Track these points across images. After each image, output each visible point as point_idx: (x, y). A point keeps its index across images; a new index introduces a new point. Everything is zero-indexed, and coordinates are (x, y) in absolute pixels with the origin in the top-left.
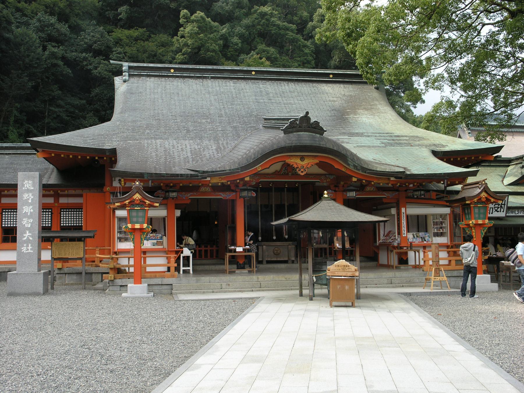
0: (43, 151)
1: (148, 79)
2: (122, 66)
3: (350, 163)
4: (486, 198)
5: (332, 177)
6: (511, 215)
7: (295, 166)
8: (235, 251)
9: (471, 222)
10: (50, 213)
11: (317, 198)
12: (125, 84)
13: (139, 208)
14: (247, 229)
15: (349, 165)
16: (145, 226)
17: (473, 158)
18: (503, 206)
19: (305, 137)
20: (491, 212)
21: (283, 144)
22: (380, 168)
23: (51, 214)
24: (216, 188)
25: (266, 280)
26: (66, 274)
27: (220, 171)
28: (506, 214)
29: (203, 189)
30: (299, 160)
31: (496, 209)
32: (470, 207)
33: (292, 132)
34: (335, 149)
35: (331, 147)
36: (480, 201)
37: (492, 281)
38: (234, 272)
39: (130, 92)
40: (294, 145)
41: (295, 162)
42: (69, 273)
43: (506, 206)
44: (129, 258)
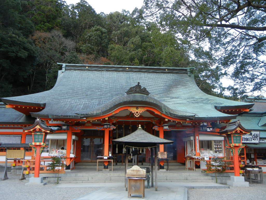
0: (9, 104)
1: (75, 71)
2: (62, 65)
3: (163, 111)
4: (39, 129)
5: (157, 119)
6: (262, 142)
7: (133, 112)
8: (102, 158)
9: (231, 145)
10: (20, 137)
11: (134, 129)
12: (63, 74)
13: (39, 134)
14: (248, 145)
15: (162, 111)
16: (42, 144)
17: (238, 110)
18: (257, 137)
19: (138, 97)
20: (251, 140)
21: (125, 100)
22: (180, 114)
23: (21, 138)
24: (94, 125)
25: (115, 176)
26: (17, 169)
27: (91, 114)
28: (259, 141)
29: (87, 125)
30: (135, 109)
31: (253, 138)
32: (231, 136)
33: (131, 94)
34: (155, 102)
35: (153, 102)
36: (236, 132)
37: (246, 180)
38: (102, 170)
39: (64, 77)
40: (131, 100)
41: (134, 110)
42: (19, 169)
43: (259, 137)
44: (44, 162)
